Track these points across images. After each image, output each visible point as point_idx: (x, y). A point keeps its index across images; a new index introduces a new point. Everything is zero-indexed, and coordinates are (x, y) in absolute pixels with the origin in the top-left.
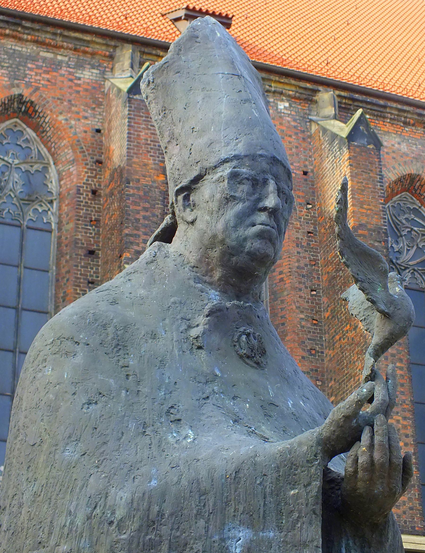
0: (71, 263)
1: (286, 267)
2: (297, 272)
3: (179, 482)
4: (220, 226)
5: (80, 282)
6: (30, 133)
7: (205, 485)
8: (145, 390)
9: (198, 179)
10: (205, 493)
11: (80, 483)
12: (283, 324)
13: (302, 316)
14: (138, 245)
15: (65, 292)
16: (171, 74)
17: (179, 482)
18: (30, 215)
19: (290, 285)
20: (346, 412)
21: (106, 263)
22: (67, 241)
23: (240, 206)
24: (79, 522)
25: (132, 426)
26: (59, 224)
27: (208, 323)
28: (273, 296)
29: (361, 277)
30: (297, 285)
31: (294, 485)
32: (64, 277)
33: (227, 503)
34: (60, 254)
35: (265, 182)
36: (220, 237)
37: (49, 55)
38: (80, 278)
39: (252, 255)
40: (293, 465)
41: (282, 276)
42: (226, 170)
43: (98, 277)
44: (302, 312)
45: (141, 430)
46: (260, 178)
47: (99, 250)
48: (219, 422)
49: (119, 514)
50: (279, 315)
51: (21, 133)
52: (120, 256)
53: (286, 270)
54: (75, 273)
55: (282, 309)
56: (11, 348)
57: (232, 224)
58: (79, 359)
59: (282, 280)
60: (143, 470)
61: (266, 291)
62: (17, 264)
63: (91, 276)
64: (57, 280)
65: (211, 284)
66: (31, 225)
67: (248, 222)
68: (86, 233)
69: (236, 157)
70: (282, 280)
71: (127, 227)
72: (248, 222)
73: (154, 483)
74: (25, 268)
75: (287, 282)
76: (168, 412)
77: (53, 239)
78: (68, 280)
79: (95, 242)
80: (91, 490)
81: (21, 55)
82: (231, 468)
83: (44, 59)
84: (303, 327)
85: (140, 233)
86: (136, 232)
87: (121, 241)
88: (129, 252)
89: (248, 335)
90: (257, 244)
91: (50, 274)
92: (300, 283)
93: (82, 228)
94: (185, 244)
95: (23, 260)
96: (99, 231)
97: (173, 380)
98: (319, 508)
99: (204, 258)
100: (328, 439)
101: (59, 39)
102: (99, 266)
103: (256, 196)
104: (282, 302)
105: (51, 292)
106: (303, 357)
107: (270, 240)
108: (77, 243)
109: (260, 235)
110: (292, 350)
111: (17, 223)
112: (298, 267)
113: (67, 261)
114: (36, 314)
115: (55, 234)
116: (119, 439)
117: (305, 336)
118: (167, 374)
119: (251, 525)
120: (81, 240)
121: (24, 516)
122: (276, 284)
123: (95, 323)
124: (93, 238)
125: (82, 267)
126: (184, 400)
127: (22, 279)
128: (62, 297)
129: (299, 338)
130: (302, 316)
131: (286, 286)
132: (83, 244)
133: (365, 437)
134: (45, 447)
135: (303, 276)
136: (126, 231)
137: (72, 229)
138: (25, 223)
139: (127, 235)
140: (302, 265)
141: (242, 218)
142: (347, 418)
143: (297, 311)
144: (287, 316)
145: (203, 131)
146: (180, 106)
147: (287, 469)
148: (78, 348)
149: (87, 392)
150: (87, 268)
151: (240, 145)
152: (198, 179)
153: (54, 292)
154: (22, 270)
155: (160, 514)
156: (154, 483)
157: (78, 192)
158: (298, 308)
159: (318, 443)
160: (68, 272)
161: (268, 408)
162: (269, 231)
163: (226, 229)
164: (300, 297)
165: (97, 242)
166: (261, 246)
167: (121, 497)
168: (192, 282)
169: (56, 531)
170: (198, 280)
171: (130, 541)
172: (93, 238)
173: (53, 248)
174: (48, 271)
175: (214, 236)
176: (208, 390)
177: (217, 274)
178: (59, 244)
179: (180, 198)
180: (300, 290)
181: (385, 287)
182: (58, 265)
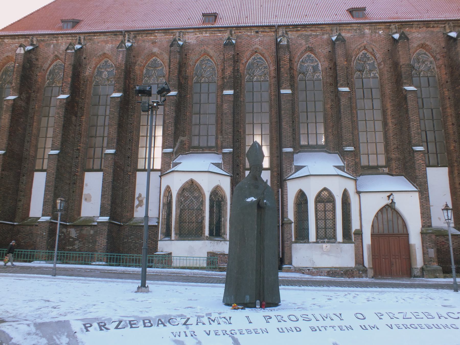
6: (313, 55)
18: (315, 77)
26: (323, 78)
37: (315, 33)
51: (310, 56)
81: (307, 35)
83: (314, 35)
101: (317, 28)
157: (326, 69)
166: (415, 44)
173: (322, 84)
178: (323, 83)
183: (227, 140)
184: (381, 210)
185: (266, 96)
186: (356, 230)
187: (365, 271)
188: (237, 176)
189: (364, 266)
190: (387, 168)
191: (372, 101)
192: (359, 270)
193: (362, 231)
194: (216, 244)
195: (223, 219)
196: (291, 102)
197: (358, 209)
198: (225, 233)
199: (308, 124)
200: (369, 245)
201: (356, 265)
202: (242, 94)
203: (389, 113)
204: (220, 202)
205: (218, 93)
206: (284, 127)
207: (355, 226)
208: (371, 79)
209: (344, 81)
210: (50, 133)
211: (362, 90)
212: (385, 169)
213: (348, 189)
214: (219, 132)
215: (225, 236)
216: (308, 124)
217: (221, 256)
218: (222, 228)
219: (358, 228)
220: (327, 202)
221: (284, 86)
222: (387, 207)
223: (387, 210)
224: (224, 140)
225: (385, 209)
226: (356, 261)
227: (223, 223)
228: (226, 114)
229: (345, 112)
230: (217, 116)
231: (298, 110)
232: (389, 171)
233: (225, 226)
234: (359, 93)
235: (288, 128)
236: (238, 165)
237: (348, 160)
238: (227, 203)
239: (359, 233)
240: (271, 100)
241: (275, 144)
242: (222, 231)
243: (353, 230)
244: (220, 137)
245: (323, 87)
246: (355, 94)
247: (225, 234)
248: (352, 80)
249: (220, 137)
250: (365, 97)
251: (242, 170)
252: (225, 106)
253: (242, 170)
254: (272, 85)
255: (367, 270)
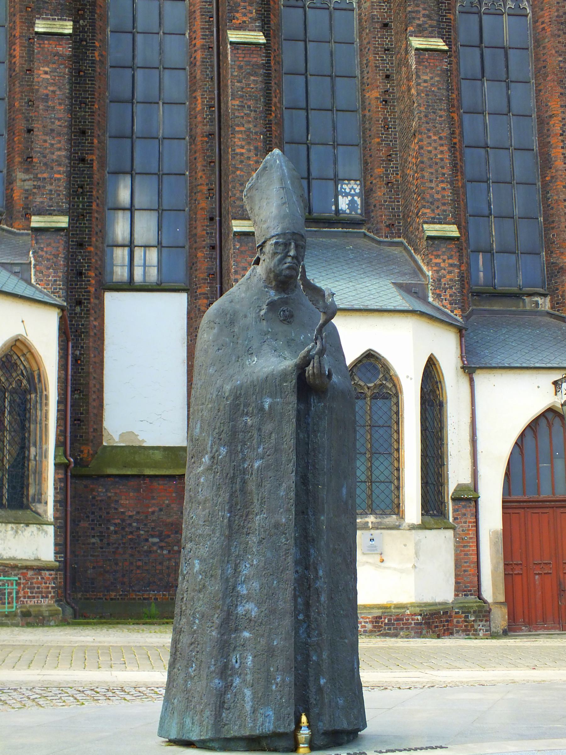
0: (371, 35)
1: (548, 17)
2: (556, 21)
3: (247, 382)
4: (272, 265)
5: (378, 51)
7: (255, 383)
8: (240, 341)
9: (264, 242)
10: (256, 386)
11: (214, 382)
12: (545, 67)
13: (560, 59)
14: (419, 19)
15: (367, 60)
16: (254, 191)
17: (247, 382)
19: (550, 33)
20: (304, 355)
21: (397, 33)
22: (366, 18)
23: (279, 256)
24: (214, 397)
25: (234, 358)
27: (267, 308)
28: (536, 44)
29: (313, 299)
30: (556, 32)
31: (286, 382)
32: (366, 48)
33: (263, 389)
34: (362, 29)
35: (290, 244)
36: (273, 269)
38: (378, 48)
39: (286, 276)
40: (286, 375)
41: (543, 26)
42: (273, 241)
43: (392, 45)
44: (560, 55)
45: (237, 359)
46: (288, 242)
47: (392, 22)
48: (268, 352)
49: (227, 394)
50: (542, 60)
52: (406, 30)
53: (547, 20)
54: (374, 44)
55: (544, 54)
56: (330, 108)
57: (277, 264)
58: (215, 331)
59: (543, 29)
60: (236, 377)
61: (531, 40)
62: (328, 40)
63: (387, 44)
64: (361, 50)
65: (271, 288)
66: (337, 6)
67: (283, 262)
68: (380, 9)
69: (277, 235)
70: (543, 29)
71: (409, 5)
72: (283, 262)
73: (238, 382)
74: (335, 42)
75: (548, 30)
76: (248, 350)
77: (355, 15)
78: (368, 50)
79: (388, 16)
80: (217, 386)
82: (265, 376)
84: (561, 68)
85: (421, 9)
86: (416, 9)
87: (406, 16)
88: (412, 26)
89: (284, 311)
90: (287, 272)
91: (355, 45)
92: (559, 30)
93: (377, 5)
94: (260, 270)
95: (333, 36)
96: (390, 6)
97: (251, 336)
98: (296, 390)
99: (268, 277)
100: (299, 364)
102: (392, 35)
103: (287, 250)
104: (544, 48)
105: (357, 60)
106: (561, 94)
107: (293, 269)
108: (374, 19)
109: (288, 268)
110: (552, 89)
111: (326, 6)
112: (557, 16)
113: (367, 34)
114: (346, 78)
115: (356, 12)
116: (228, 364)
117: (563, 76)
118: (249, 333)
119: (271, 397)
120: (377, 16)
121: (198, 393)
122: (539, 33)
123: (223, 313)
124: (386, 12)
125: (379, 38)
126: (255, 344)
127: (333, 52)
128: (366, 64)
129: (558, 78)
130: (560, 59)
131: (547, 34)
132: (379, 19)
133: (312, 363)
134: (204, 367)
135: (562, 24)
136: (409, 9)
137: (369, 7)
138: (332, 6)
139: (410, 11)
140: (561, 14)
141: (281, 261)
142: (304, 357)
143: (556, 54)
144: (548, 60)
145: (265, 221)
146: (257, 208)
147: (284, 375)
148: (216, 325)
149: (218, 345)
150: (383, 38)
151: (279, 229)
152: (264, 242)
153: (359, 60)
154: (333, 45)
155: (240, 394)
156: (238, 382)
158: (556, 52)
159: (295, 366)
160: (369, 43)
161: (290, 343)
162: (292, 266)
163: (274, 266)
164: (559, 42)
165: (389, 16)
167: (227, 387)
168: (263, 288)
169: (207, 399)
170: (266, 287)
171: (230, 404)
172: (386, 12)
174: (353, 43)
175: (270, 269)
176: (266, 338)
177: (274, 284)
179: (259, 249)
180: (559, 36)
181: (324, 301)
182: (360, 37)
183: (48, 187)
184: (533, 426)
185: (175, 51)
186: (460, 488)
187: (484, 612)
188: (78, 309)
189: (480, 597)
190: (548, 299)
191: (508, 88)
192: (466, 611)
193: (476, 489)
194: (10, 533)
195: (33, 450)
196: (262, 71)
197: (468, 420)
198: (39, 498)
199: (308, 149)
200: (495, 532)
201: (456, 595)
202: (99, 37)
203: (557, 129)
204: (27, 392)
205: (13, 28)
206: (238, 150)
207: (457, 474)
208: (505, 18)
209: (429, 17)
210: (82, 638)
211: (302, 78)
212: (540, 300)
213: (553, 381)
214: (17, 159)
215: (40, 508)
216: (308, 149)
217: (30, 573)
218: (31, 480)
219: (466, 479)
220: (374, 397)
221: (240, 17)
222: (550, 416)
223: (550, 425)
224: (39, 187)
225: (543, 423)
226: (457, 583)
227: (32, 464)
228: (46, 99)
229: (432, 116)
230: (11, 106)
231: (281, 101)
232: (552, 307)
233: (39, 474)
234: (469, 60)
235: (252, 154)
236: (80, 274)
237: (437, 264)
238: (47, 397)
239: (469, 499)
240: (193, 64)
241: (203, 204)
242: (32, 491)
243: (451, 488)
244: (20, 175)
245: (360, 33)
246: (458, 63)
247: (40, 501)
248: (452, 17)
249: (20, 175)
250: (487, 73)
251: (92, 290)
252: (44, 73)
253: (92, 290)
254: (198, 14)
255: (489, 611)
